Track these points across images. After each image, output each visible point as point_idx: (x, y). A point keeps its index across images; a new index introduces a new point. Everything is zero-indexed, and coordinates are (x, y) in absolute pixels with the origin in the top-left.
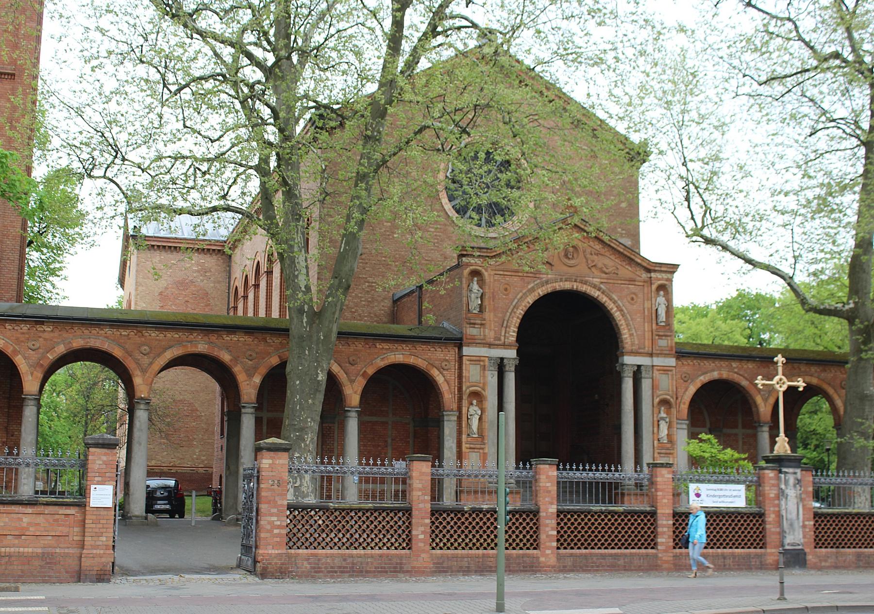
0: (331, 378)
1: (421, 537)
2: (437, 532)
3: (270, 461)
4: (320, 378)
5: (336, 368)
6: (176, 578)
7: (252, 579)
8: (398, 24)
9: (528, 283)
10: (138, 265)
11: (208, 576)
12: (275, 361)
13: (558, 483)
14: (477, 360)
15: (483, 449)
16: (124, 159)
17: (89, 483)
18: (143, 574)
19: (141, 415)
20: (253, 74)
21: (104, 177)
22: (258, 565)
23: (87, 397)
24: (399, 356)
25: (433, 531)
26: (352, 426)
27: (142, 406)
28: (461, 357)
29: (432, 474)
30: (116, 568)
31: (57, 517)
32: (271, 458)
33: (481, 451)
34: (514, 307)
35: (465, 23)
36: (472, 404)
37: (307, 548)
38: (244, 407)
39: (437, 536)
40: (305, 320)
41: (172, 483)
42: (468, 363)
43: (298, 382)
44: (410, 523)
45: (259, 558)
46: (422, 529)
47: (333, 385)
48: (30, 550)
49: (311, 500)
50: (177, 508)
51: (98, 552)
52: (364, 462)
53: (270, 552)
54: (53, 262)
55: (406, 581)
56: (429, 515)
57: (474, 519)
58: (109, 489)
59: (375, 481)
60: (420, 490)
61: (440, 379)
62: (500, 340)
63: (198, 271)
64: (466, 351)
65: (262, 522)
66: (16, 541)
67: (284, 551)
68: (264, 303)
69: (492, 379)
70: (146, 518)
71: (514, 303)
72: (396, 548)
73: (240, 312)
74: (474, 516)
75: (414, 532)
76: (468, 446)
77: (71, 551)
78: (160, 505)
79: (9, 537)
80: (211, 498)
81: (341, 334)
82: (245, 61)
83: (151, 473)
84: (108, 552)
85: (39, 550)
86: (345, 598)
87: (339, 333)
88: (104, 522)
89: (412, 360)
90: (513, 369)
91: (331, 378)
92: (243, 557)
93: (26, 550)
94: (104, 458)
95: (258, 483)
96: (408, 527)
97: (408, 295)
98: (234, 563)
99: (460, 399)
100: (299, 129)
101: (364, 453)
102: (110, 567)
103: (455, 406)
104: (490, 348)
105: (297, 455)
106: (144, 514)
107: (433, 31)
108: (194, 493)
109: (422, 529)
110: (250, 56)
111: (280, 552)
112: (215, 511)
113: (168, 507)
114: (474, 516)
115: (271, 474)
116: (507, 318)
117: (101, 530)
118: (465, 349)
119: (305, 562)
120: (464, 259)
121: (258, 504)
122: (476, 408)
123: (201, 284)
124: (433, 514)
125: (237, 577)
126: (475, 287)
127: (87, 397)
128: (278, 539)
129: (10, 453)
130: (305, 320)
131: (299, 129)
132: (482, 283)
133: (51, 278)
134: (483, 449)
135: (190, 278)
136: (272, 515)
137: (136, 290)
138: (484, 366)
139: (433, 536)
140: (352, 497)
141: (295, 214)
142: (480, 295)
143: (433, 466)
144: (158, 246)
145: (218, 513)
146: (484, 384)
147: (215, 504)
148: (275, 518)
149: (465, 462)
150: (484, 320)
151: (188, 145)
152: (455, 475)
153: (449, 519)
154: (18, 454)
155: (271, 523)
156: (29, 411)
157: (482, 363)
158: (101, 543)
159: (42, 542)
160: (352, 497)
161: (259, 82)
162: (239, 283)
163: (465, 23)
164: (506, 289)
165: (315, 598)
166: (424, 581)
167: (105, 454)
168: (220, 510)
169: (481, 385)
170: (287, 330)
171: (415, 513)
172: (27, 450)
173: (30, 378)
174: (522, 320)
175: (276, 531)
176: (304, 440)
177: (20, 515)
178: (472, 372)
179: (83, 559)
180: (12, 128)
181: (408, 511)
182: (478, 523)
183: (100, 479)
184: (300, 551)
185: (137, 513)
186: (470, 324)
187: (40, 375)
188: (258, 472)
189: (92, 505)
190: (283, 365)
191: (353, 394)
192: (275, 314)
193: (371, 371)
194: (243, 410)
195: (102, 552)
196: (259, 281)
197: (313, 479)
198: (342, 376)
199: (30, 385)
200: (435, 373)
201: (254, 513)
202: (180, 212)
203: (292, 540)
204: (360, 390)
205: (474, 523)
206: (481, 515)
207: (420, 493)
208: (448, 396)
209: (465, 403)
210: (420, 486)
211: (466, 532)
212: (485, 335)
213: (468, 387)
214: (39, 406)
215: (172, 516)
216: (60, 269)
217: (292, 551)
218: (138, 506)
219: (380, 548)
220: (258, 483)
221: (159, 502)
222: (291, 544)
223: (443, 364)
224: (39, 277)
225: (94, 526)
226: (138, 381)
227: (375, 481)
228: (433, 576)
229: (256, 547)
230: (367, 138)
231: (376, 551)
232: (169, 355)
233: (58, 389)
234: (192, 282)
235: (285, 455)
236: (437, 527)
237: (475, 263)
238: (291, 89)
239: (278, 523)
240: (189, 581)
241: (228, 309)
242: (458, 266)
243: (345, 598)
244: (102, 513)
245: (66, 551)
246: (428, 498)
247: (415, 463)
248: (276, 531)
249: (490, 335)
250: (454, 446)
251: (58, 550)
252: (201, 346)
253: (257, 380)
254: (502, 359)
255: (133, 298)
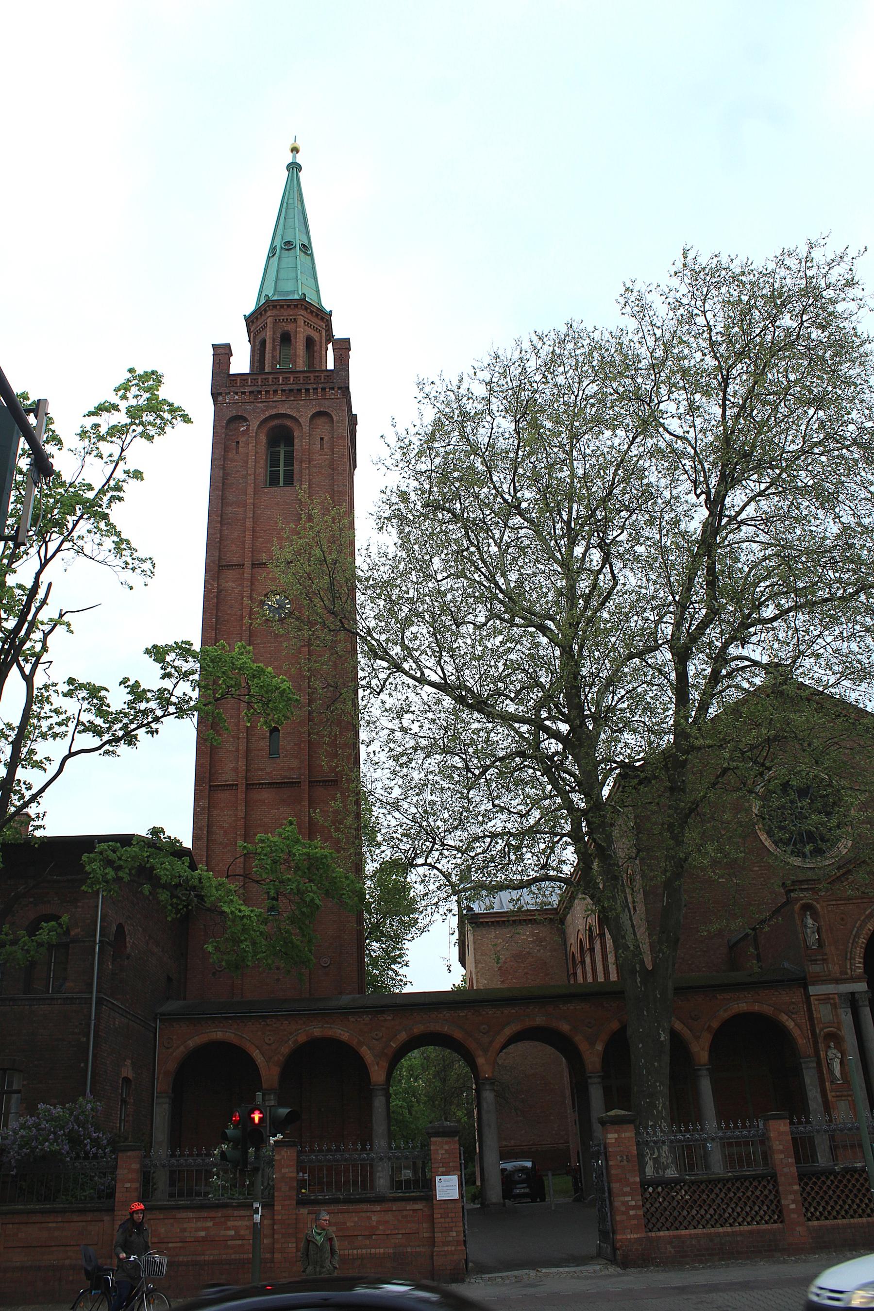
0: (674, 1035)
1: (793, 1206)
2: (809, 1199)
3: (616, 1136)
4: (662, 1039)
5: (678, 1026)
6: (533, 1273)
7: (612, 1270)
8: (682, 675)
9: (865, 910)
10: (474, 943)
11: (566, 1269)
12: (615, 1025)
13: (794, 1140)
14: (826, 999)
15: (851, 1096)
16: (443, 845)
17: (433, 1175)
18: (500, 1271)
19: (488, 1096)
20: (553, 746)
21: (426, 864)
22: (618, 1252)
23: (444, 1081)
24: (742, 1005)
25: (805, 1199)
26: (706, 1086)
27: (487, 1087)
28: (808, 997)
29: (792, 1133)
30: (470, 1265)
31: (405, 1213)
32: (616, 1132)
33: (849, 1098)
34: (855, 936)
35: (747, 663)
36: (830, 1047)
37: (668, 1230)
38: (590, 1077)
39: (810, 1204)
40: (639, 980)
41: (529, 1164)
42: (816, 1003)
43: (640, 1046)
44: (777, 1191)
45: (618, 1245)
46: (791, 1197)
47: (678, 1044)
48: (382, 1250)
49: (671, 1173)
50: (537, 1192)
51: (449, 1248)
52: (723, 1125)
53: (629, 1236)
54: (393, 949)
55: (785, 1262)
56: (797, 1181)
57: (849, 1181)
58: (454, 1180)
59: (738, 1144)
60: (782, 1152)
61: (790, 1024)
62: (846, 973)
63: (532, 942)
64: (813, 990)
65: (616, 1204)
66: (368, 1242)
67: (644, 1235)
68: (601, 967)
69: (846, 1018)
70: (504, 1205)
71: (854, 933)
72: (766, 1223)
73: (580, 979)
74: (848, 1177)
75: (783, 1202)
76: (833, 1094)
77: (422, 1249)
78: (521, 1189)
79: (360, 1238)
80: (570, 1178)
81: (678, 990)
82: (543, 735)
83: (505, 1155)
84: (459, 1248)
85: (391, 1251)
86: (714, 1288)
87: (676, 989)
88: (453, 1215)
89: (756, 1008)
90: (867, 1003)
91: (674, 1035)
92: (602, 1244)
93: (377, 1250)
94: (446, 1147)
95: (607, 1160)
96: (776, 1197)
97: (742, 939)
98: (594, 1251)
99: (816, 1043)
100: (606, 792)
101: (721, 1115)
102: (462, 1264)
103: (811, 1051)
104: (837, 984)
105: (651, 1123)
106: (502, 1200)
107: (715, 678)
108: (550, 1174)
109: (791, 1197)
110: (547, 730)
111: (639, 1236)
112: (576, 1192)
113: (527, 1190)
114: (848, 1177)
115: (618, 1149)
116: (849, 949)
117: (451, 1225)
118: (810, 988)
119: (668, 1246)
120: (792, 894)
121: (609, 1183)
122: (835, 1051)
123: (539, 955)
124: (801, 1179)
125: (598, 1267)
126: (810, 921)
127: (444, 1081)
128: (635, 1222)
129: (364, 1149)
130: (639, 980)
131: (606, 792)
132: (815, 916)
133: (393, 966)
134: (851, 1096)
135: (527, 950)
136: (625, 1194)
137: (476, 967)
138: (835, 1004)
139: (806, 1205)
140: (718, 1167)
141: (612, 876)
142: (815, 930)
143: (792, 1123)
144: (492, 922)
145: (579, 1193)
146: (839, 1023)
147: (575, 1184)
148: (629, 1198)
149: (835, 1115)
150: (826, 954)
151: (497, 824)
152: (826, 1131)
153: (829, 1183)
154: (371, 1149)
155: (625, 1203)
156: (379, 1102)
157: (832, 1001)
158: (451, 1239)
159: (393, 1241)
160: (718, 1167)
161: (557, 753)
162: (575, 949)
163: (747, 663)
164: (842, 919)
165: (682, 1290)
166: (805, 1261)
167: (447, 1143)
168: (582, 1189)
169: (836, 1025)
170: (622, 992)
171: (781, 1179)
172: (380, 1143)
173: (376, 1068)
174: (866, 949)
175: (632, 1213)
176: (656, 1107)
177: (368, 1214)
178: (823, 1012)
179: (435, 1258)
180: (337, 830)
181: (773, 1178)
182: (854, 1186)
183: (443, 1169)
184: (662, 1233)
185: (494, 1201)
186: (811, 961)
187: (385, 1065)
188: (605, 1148)
189: (438, 1198)
190: (623, 1029)
191: (701, 1051)
192: (613, 977)
193: (715, 1025)
194: (589, 1081)
195: (453, 1248)
196: (593, 944)
197: (672, 1149)
198: (686, 1033)
199: (377, 1075)
200: (784, 1018)
201: (607, 1194)
202: (501, 887)
203: (651, 1221)
204: (707, 1045)
205: (850, 1186)
206: (856, 1176)
207: (782, 1156)
208: (802, 1041)
209: (821, 1046)
210: (781, 1147)
211: (843, 1196)
212: (829, 971)
213: (821, 1030)
214: (388, 1096)
215: (534, 1201)
216: (400, 956)
217: (653, 1234)
218: (495, 1194)
219: (749, 1224)
220: (607, 1160)
221: (518, 1186)
222: (650, 1226)
223: (791, 1008)
224: (381, 966)
225: (442, 1220)
226: (480, 1061)
227: (738, 1144)
228: (815, 1253)
229: (614, 1233)
230: (672, 789)
231: (745, 1228)
232: (508, 1032)
233: (416, 1074)
234: (528, 953)
235: (632, 1127)
236: (809, 1194)
237: (805, 897)
238: (590, 755)
239: (633, 1203)
240: (546, 1275)
241: (569, 976)
242: (788, 902)
243: (714, 1288)
244: (449, 1206)
245: (418, 1249)
246: (791, 1160)
247: (771, 1123)
248: (632, 1213)
249: (835, 970)
250: (819, 1096)
251: (409, 1250)
252: (540, 1020)
253: (600, 1047)
254: (853, 994)
255: (474, 976)
